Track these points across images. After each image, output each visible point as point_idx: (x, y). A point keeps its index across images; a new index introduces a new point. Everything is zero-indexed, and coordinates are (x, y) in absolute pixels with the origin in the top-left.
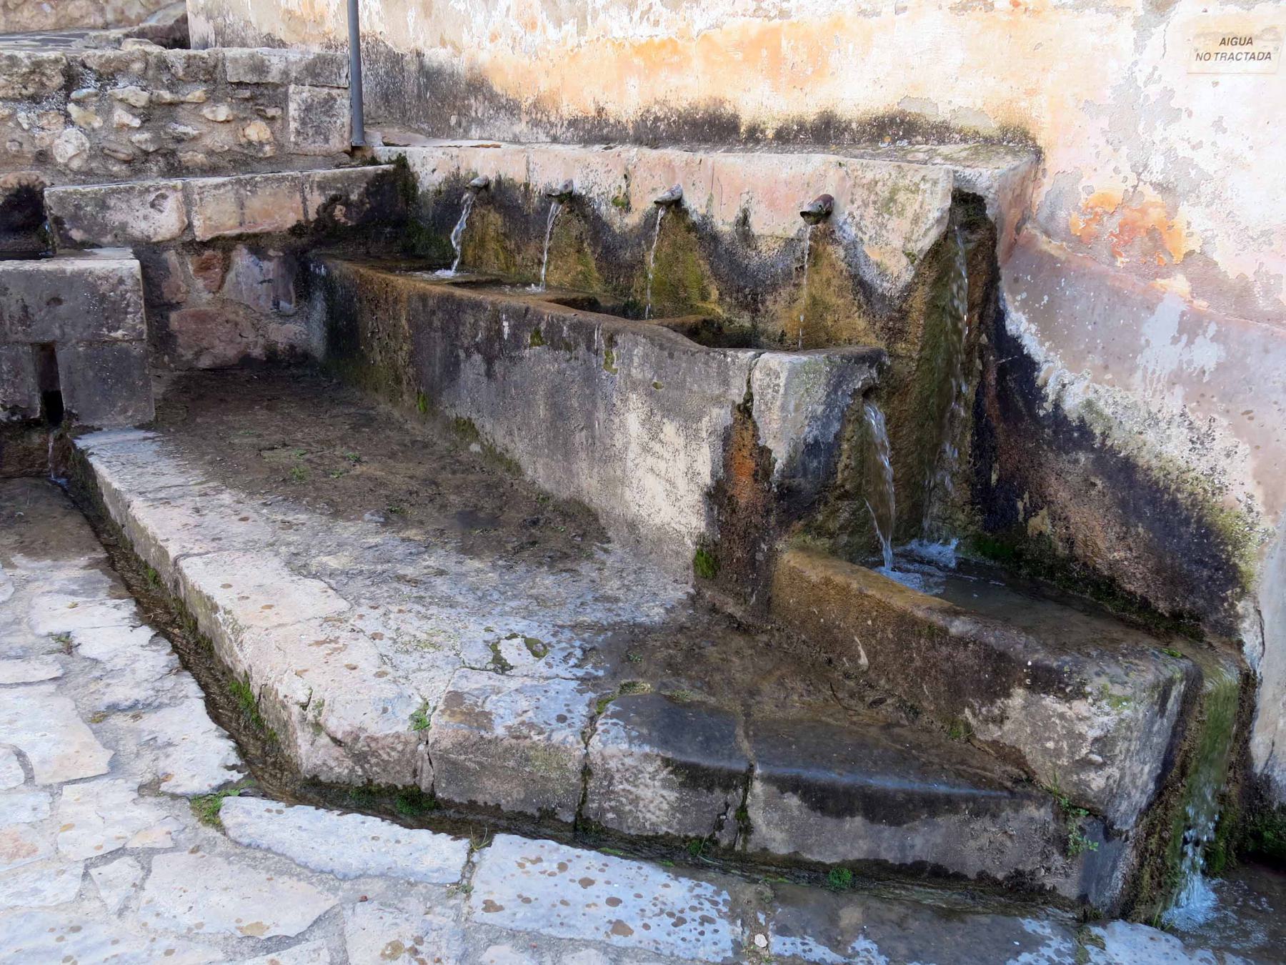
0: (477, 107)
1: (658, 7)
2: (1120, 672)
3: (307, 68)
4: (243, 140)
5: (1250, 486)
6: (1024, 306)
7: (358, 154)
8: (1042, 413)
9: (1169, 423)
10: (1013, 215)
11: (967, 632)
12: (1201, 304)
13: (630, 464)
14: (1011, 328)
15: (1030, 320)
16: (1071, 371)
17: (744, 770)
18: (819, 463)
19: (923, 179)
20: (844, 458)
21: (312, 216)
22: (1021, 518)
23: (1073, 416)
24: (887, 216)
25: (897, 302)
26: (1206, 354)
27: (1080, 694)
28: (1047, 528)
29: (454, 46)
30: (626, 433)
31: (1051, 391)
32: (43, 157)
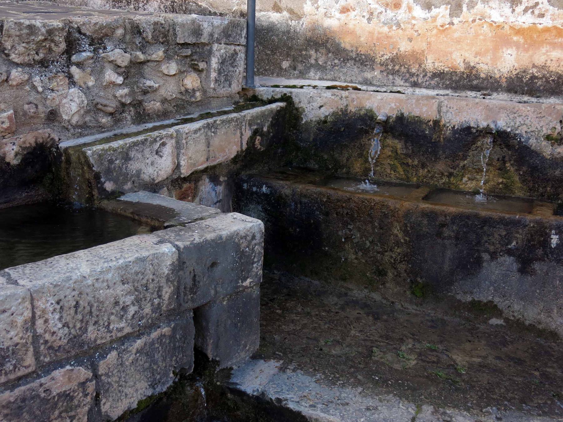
1: (544, 4)
4: (183, 89)
21: (245, 147)
32: (53, 116)
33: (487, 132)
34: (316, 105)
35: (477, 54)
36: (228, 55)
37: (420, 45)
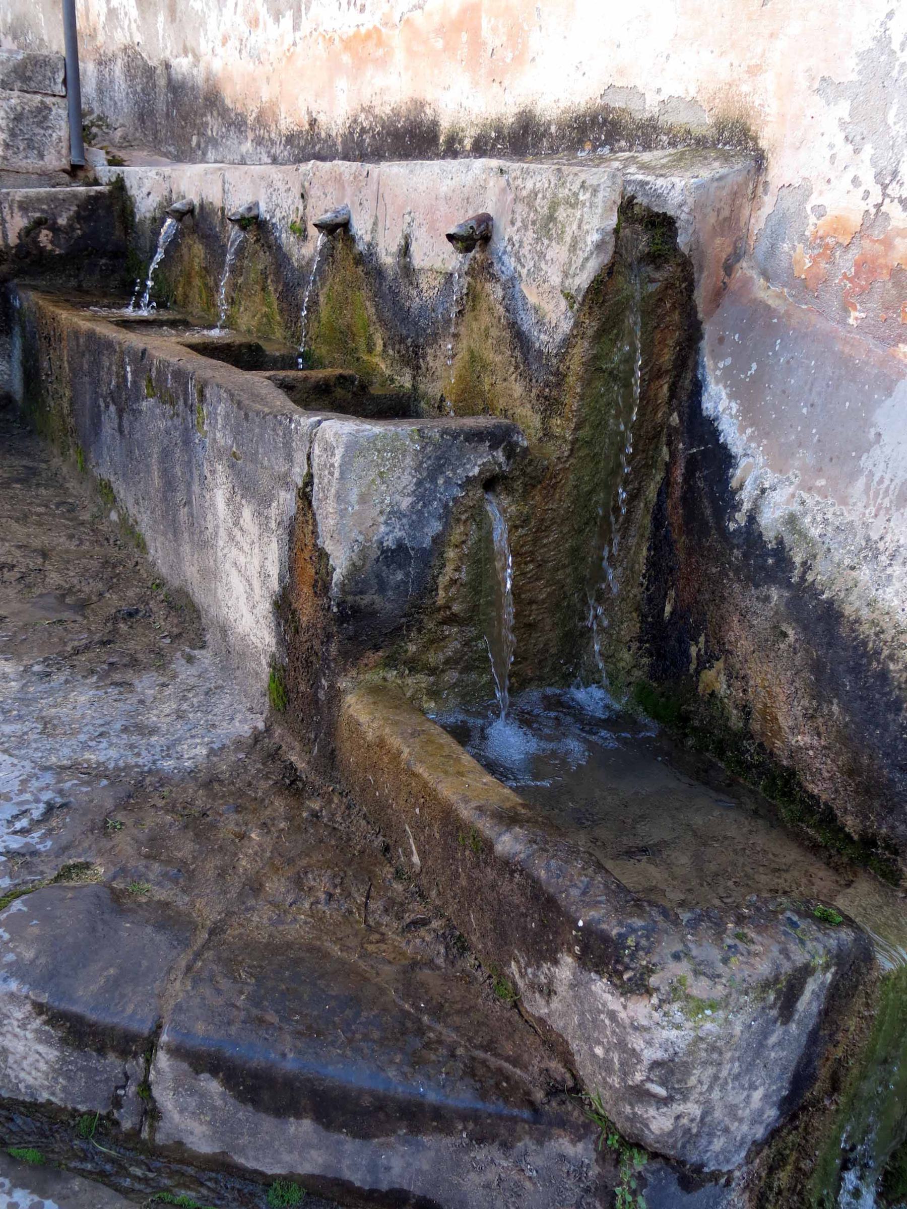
0: (213, 124)
2: (715, 954)
3: (15, 70)
6: (728, 377)
7: (81, 174)
8: (732, 526)
9: (892, 557)
10: (719, 248)
11: (515, 854)
13: (220, 554)
14: (708, 406)
15: (731, 396)
16: (774, 472)
17: (146, 1032)
18: (407, 575)
19: (583, 186)
20: (449, 568)
21: (13, 240)
22: (693, 667)
23: (769, 536)
24: (546, 242)
25: (554, 361)
27: (638, 987)
28: (721, 688)
29: (195, 55)
30: (215, 515)
31: (746, 496)
36: (27, 108)
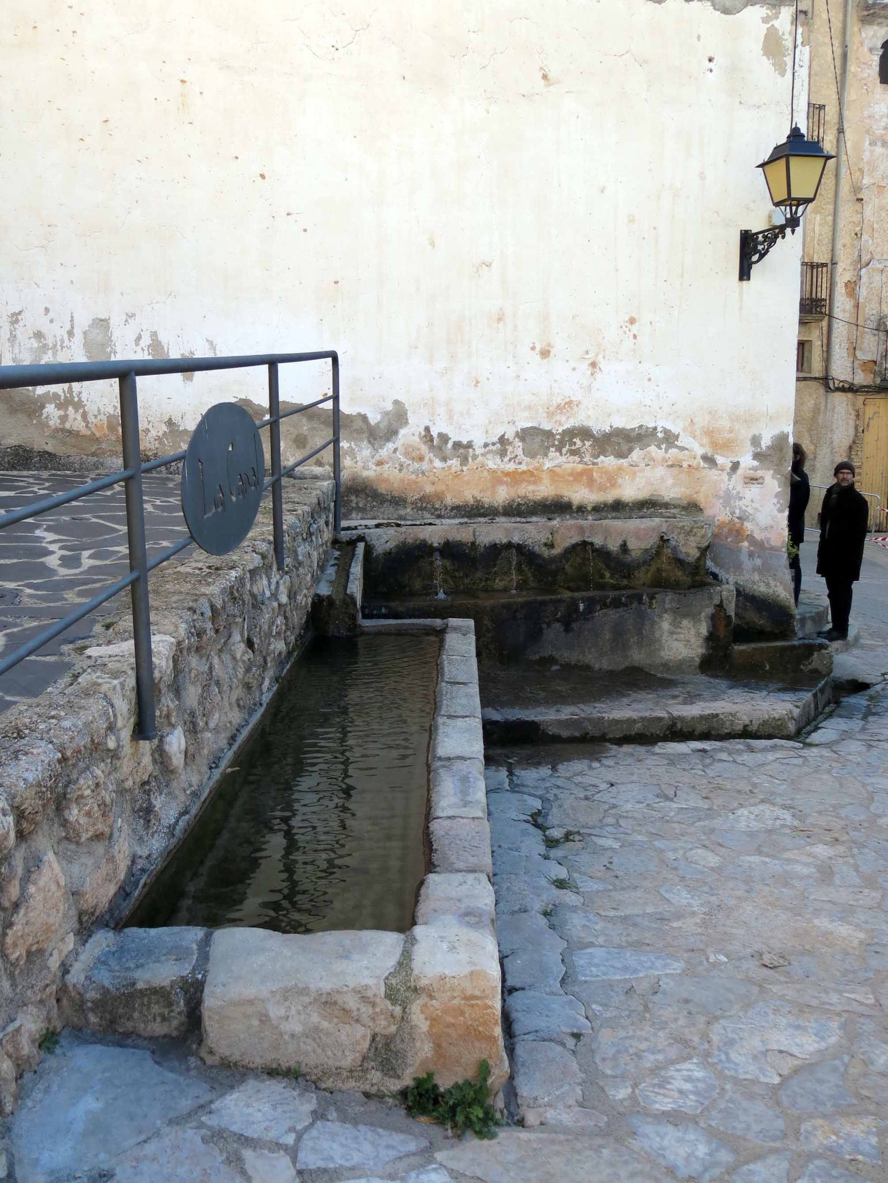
5: (784, 593)
12: (752, 548)
13: (664, 641)
26: (758, 562)
33: (509, 545)
34: (383, 541)
35: (481, 491)
37: (440, 487)
